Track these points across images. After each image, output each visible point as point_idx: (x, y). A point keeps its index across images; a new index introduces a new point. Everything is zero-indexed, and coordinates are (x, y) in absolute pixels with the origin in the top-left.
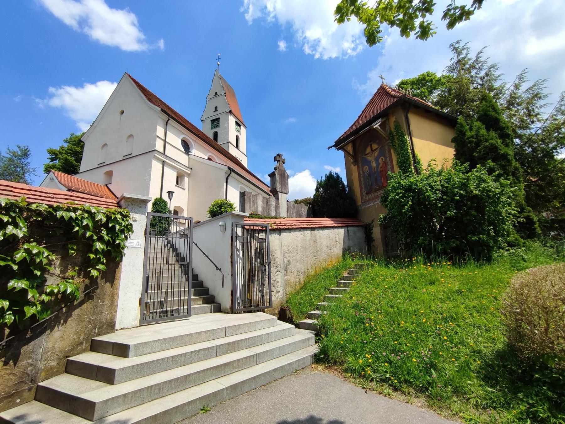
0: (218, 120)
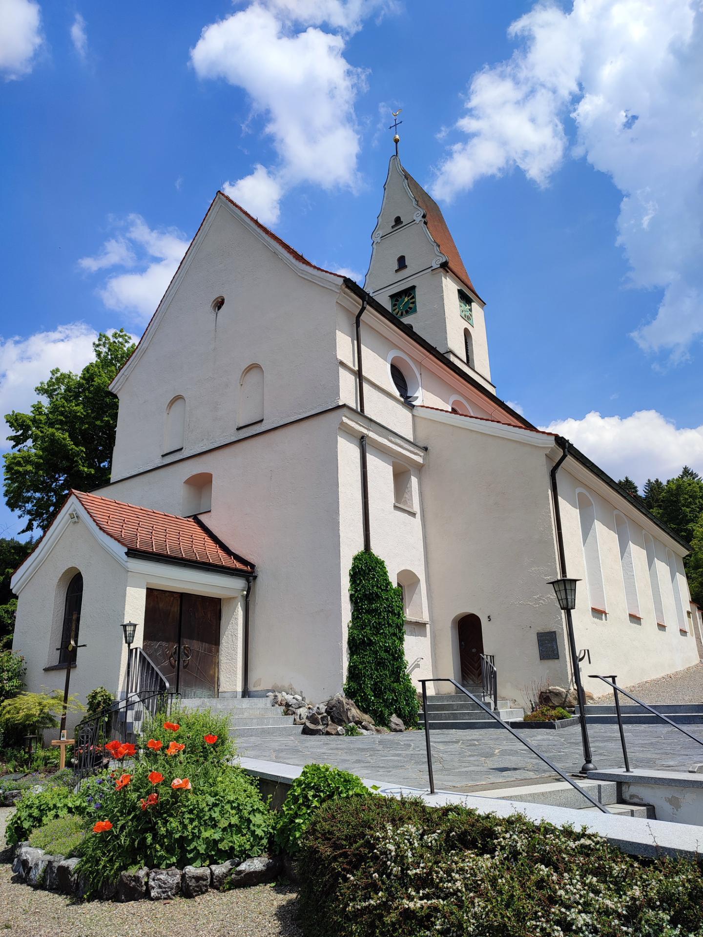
0: (410, 291)
